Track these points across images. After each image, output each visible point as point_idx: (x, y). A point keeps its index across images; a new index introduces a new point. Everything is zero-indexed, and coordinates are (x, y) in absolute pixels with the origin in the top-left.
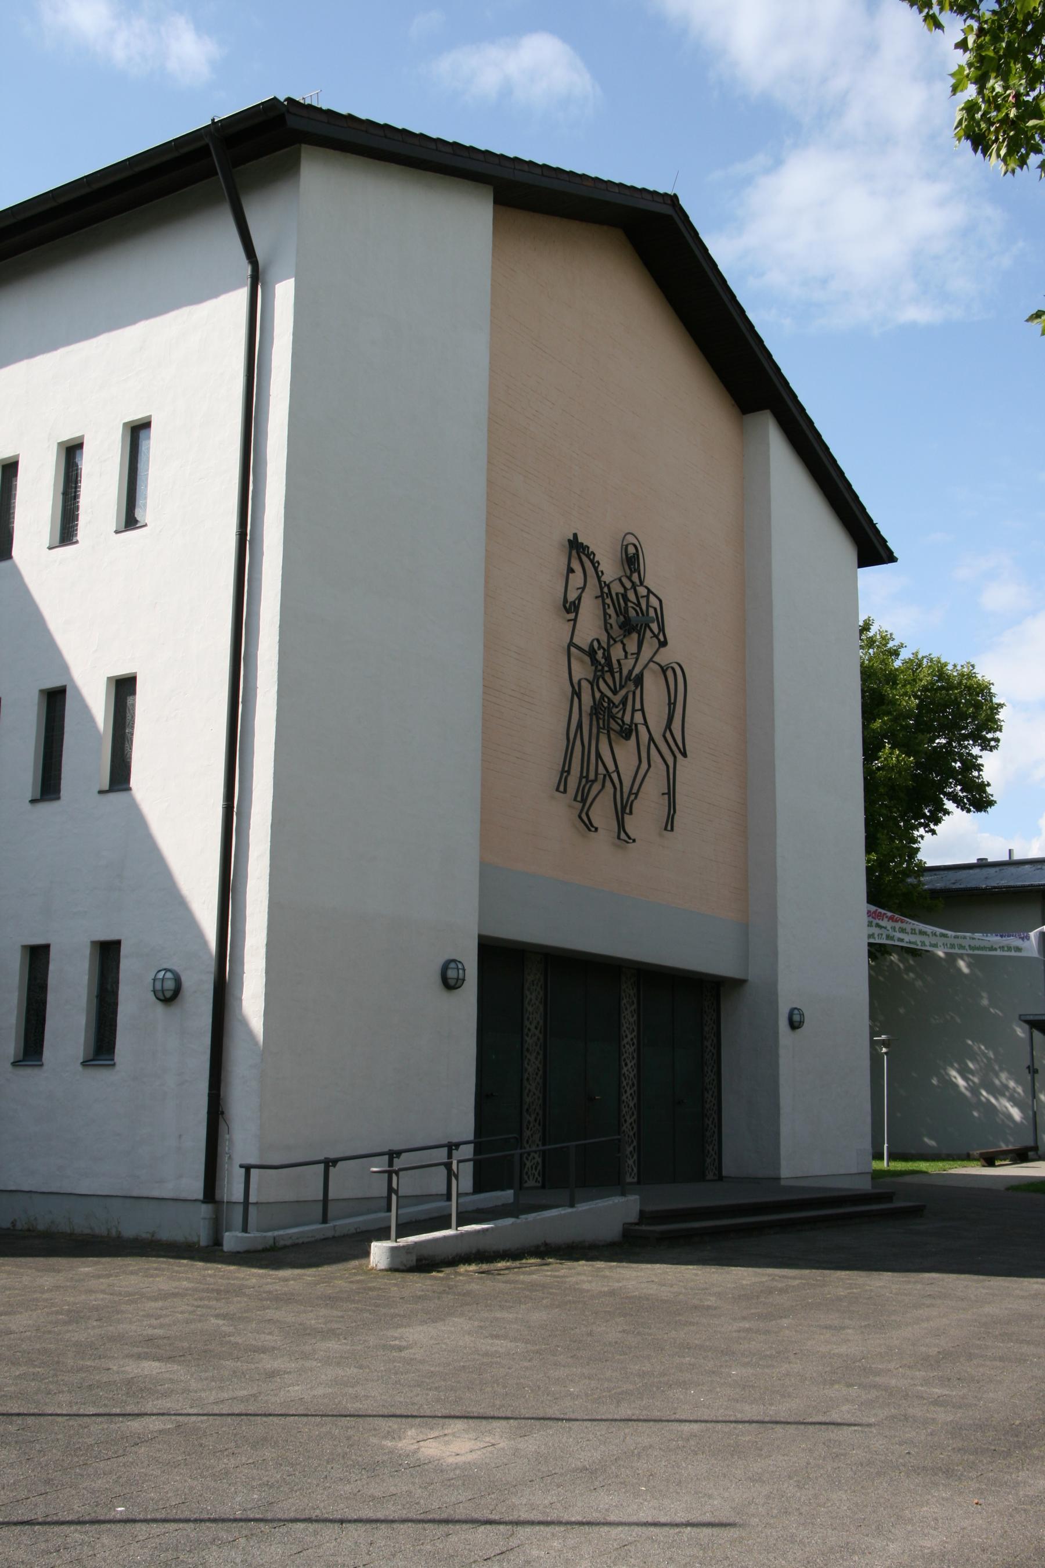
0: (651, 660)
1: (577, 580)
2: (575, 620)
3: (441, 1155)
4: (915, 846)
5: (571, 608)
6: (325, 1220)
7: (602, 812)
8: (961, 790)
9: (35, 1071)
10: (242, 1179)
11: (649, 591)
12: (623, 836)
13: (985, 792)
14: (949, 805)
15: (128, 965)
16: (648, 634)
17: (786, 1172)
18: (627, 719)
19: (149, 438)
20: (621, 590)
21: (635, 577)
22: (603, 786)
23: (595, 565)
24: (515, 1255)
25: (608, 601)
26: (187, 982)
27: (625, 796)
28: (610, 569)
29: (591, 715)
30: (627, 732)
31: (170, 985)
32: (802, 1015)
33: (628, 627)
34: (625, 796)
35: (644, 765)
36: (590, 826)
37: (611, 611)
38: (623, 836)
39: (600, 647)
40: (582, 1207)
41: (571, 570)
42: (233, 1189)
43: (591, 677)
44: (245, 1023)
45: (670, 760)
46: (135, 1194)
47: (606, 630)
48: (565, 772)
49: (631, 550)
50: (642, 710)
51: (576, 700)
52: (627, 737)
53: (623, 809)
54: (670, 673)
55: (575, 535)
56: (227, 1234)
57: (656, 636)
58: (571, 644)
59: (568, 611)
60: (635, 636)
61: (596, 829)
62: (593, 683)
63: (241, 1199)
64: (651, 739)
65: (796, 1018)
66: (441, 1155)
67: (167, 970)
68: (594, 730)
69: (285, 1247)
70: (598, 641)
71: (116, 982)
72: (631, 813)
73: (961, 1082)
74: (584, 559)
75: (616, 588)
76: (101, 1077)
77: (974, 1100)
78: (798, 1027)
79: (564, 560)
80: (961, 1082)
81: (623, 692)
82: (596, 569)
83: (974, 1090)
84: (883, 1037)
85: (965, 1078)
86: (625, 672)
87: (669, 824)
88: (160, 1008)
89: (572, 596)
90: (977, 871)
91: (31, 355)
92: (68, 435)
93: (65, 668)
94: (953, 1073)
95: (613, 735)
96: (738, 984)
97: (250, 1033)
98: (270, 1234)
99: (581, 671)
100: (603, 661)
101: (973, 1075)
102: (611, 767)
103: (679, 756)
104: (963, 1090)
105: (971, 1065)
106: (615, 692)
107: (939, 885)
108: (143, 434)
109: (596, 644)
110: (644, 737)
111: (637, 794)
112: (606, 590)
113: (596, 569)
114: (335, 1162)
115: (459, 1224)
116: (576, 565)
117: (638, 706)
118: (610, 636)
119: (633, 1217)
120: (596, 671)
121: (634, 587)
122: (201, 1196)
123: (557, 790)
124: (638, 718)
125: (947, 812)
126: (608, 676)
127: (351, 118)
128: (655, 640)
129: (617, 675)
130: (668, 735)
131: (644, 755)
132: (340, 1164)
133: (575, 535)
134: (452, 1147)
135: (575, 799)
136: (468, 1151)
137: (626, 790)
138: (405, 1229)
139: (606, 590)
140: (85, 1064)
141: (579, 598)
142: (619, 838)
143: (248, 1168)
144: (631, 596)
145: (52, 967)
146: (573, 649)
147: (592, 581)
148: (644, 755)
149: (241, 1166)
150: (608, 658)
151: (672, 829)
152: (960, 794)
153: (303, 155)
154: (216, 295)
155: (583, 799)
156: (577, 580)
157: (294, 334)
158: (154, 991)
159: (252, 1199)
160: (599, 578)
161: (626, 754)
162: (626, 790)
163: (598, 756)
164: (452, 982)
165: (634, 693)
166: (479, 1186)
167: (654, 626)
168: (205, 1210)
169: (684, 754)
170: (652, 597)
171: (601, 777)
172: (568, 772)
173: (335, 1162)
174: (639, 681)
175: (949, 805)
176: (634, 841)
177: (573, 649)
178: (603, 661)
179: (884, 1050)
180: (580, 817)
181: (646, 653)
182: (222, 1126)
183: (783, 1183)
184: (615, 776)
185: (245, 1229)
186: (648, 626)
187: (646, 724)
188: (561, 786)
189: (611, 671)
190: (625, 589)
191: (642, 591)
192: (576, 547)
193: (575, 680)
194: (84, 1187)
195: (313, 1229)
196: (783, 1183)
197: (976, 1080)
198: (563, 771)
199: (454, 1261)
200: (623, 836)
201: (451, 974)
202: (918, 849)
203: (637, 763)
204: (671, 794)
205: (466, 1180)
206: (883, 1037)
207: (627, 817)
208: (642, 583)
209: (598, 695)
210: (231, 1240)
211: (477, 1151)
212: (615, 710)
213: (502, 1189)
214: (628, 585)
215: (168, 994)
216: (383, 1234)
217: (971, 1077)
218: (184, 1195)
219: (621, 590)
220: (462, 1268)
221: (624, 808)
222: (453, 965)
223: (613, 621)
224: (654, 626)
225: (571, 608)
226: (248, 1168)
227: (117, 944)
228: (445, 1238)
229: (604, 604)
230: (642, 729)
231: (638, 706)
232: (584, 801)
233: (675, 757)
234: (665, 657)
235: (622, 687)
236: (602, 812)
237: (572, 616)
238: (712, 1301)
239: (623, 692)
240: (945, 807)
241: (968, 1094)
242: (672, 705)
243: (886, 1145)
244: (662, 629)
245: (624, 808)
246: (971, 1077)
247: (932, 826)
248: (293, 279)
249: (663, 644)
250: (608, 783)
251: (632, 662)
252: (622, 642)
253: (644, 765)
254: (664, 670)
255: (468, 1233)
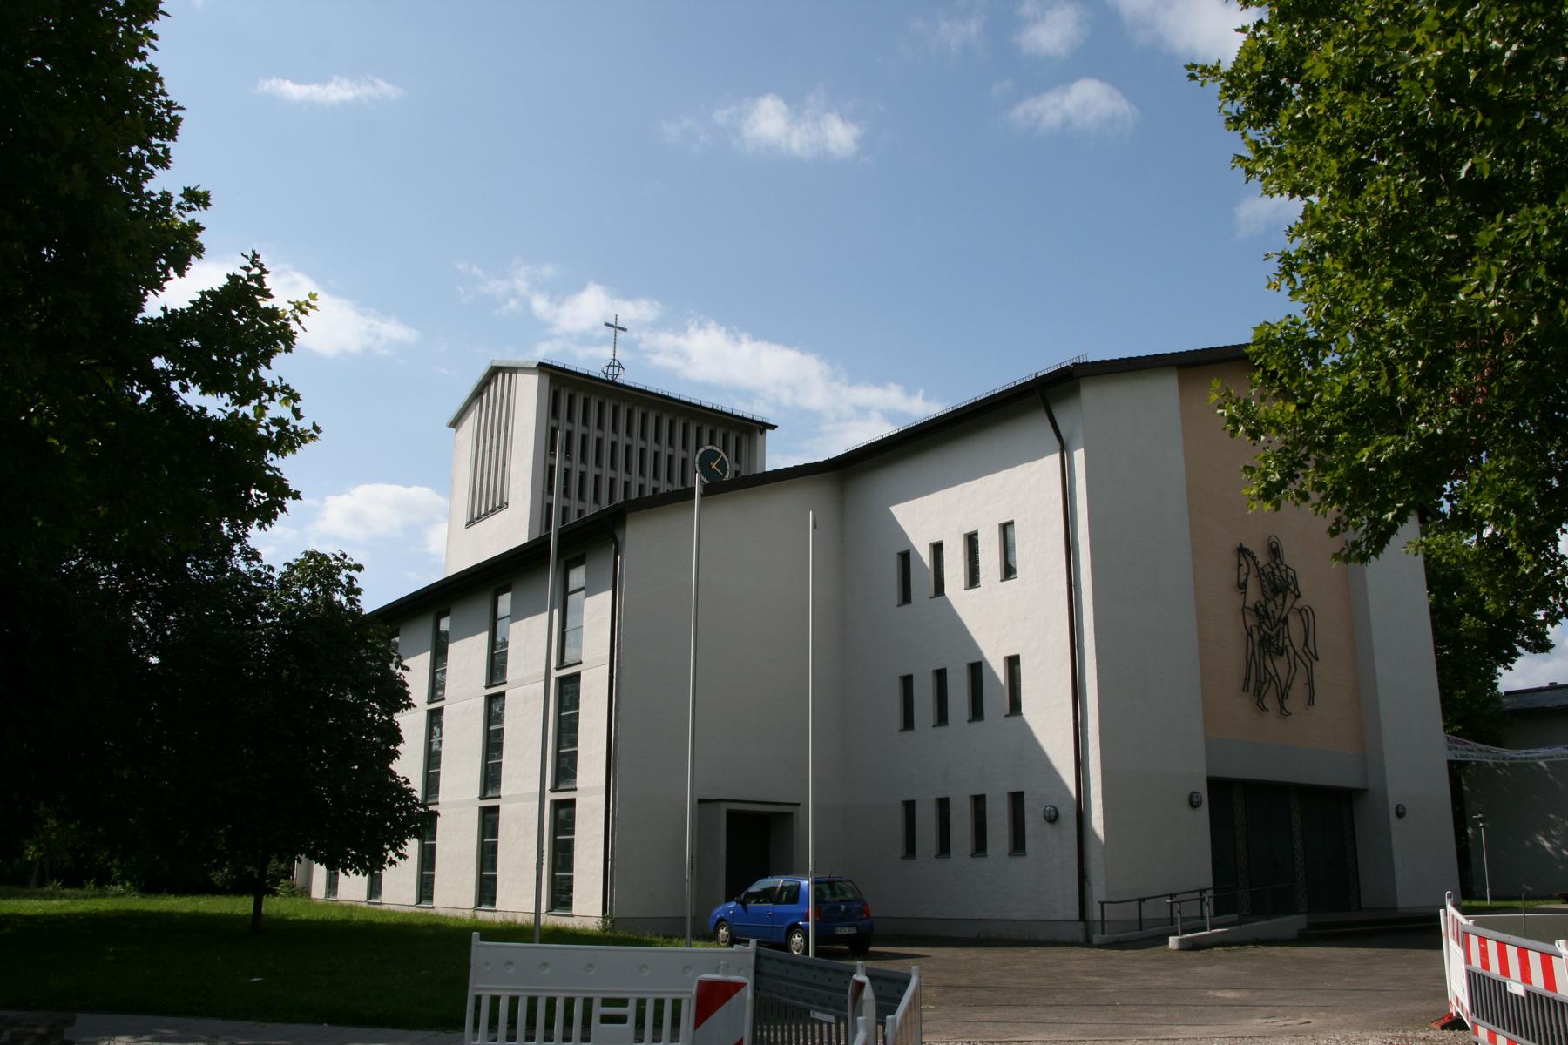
0: (1292, 607)
1: (1244, 569)
2: (1245, 593)
3: (1197, 895)
4: (1495, 681)
5: (1242, 586)
6: (1140, 930)
7: (1270, 701)
8: (1528, 639)
9: (983, 859)
10: (1100, 909)
11: (1287, 567)
12: (1284, 712)
13: (1546, 638)
14: (1520, 649)
15: (1029, 804)
16: (1288, 592)
17: (1401, 904)
18: (1280, 644)
19: (1013, 530)
20: (1270, 570)
21: (1278, 561)
22: (1270, 684)
23: (1254, 558)
24: (1242, 944)
25: (1263, 578)
26: (1062, 811)
27: (1283, 688)
28: (1262, 558)
29: (1259, 645)
30: (1281, 652)
31: (1053, 814)
32: (1404, 809)
33: (1276, 590)
34: (1283, 688)
35: (1293, 669)
36: (1264, 709)
37: (1266, 584)
38: (1283, 711)
39: (1261, 605)
40: (1275, 920)
41: (1240, 565)
42: (1095, 914)
43: (1256, 624)
44: (1093, 832)
45: (1309, 665)
46: (1042, 918)
47: (1264, 595)
48: (1247, 680)
49: (1274, 545)
50: (1289, 637)
51: (1250, 639)
52: (1282, 655)
53: (1282, 696)
54: (1304, 613)
55: (1241, 545)
56: (1094, 936)
57: (1294, 593)
58: (1244, 607)
59: (1241, 589)
60: (1281, 595)
61: (1268, 710)
62: (1259, 627)
63: (1100, 919)
64: (1296, 653)
65: (1401, 811)
66: (1197, 895)
67: (1051, 806)
68: (1262, 653)
69: (1123, 942)
70: (1259, 602)
71: (1023, 813)
72: (1287, 698)
73: (1547, 845)
74: (1247, 556)
75: (1268, 569)
76: (1018, 861)
77: (1558, 857)
78: (1403, 816)
79: (1236, 559)
80: (1547, 845)
81: (1275, 630)
82: (1254, 561)
83: (1558, 850)
84: (1480, 815)
85: (1551, 842)
86: (1277, 617)
87: (1311, 701)
88: (1048, 826)
89: (1242, 579)
90: (1548, 692)
91: (944, 488)
92: (969, 530)
93: (980, 652)
94: (1541, 838)
95: (1273, 655)
96: (1365, 790)
97: (1096, 836)
98: (1116, 936)
99: (1251, 621)
100: (1263, 613)
101: (1557, 839)
102: (1273, 673)
103: (1313, 660)
104: (1549, 850)
105: (1554, 833)
106: (1272, 630)
107: (1519, 705)
108: (1009, 528)
109: (1258, 604)
110: (1291, 652)
111: (1290, 687)
112: (1261, 572)
113: (1254, 561)
114: (1144, 900)
115: (1211, 929)
116: (1243, 561)
117: (1286, 635)
118: (1266, 598)
119: (1304, 926)
120: (1260, 619)
121: (1278, 567)
122: (1078, 918)
123: (1244, 690)
124: (1287, 642)
125: (1519, 655)
126: (1267, 622)
127: (1103, 361)
128: (1293, 595)
129: (1272, 620)
130: (1306, 650)
131: (1292, 662)
132: (1147, 901)
133: (1241, 545)
134: (1202, 891)
135: (1254, 694)
136: (1210, 893)
137: (1283, 685)
138: (1184, 932)
139: (1261, 572)
140: (972, 856)
141: (1246, 580)
142: (1281, 713)
143: (1102, 904)
144: (1277, 572)
145: (987, 806)
146: (1246, 610)
147: (1253, 567)
148: (1292, 662)
149: (1099, 902)
150: (1266, 611)
151: (1313, 704)
152: (1527, 641)
153: (1082, 385)
154: (1042, 457)
155: (1259, 695)
156: (1244, 569)
157: (1087, 477)
158: (1045, 817)
159: (1105, 919)
160: (1257, 566)
161: (1281, 665)
162: (1283, 685)
163: (1266, 668)
164: (1195, 804)
165: (1283, 628)
166: (1218, 912)
167: (1292, 588)
168: (1081, 925)
169: (1317, 659)
170: (1289, 570)
171: (1268, 680)
172: (1249, 680)
173: (1144, 900)
174: (1286, 621)
175: (1520, 649)
176: (1290, 714)
177: (1246, 610)
178: (1263, 613)
179: (1481, 824)
180: (1257, 704)
181: (1288, 603)
182: (1086, 884)
183: (1399, 910)
184: (1276, 678)
185: (1103, 933)
186: (1288, 587)
187: (1292, 645)
188: (1246, 688)
189: (1269, 618)
190: (1273, 569)
191: (1283, 568)
192: (1242, 551)
193: (1248, 626)
194: (1014, 916)
195: (1135, 934)
196: (1399, 910)
197: (1558, 842)
198: (1246, 679)
199: (1211, 946)
200: (1283, 711)
201: (1195, 799)
202: (1497, 684)
203: (1288, 668)
204: (1310, 684)
205: (1209, 911)
206: (1480, 815)
207: (1286, 701)
208: (1282, 563)
209: (1262, 633)
210: (1096, 938)
211: (1214, 893)
212: (1273, 641)
213: (1229, 913)
214: (1274, 566)
215: (1053, 818)
216: (1175, 934)
217: (1554, 841)
218: (1068, 918)
219: (1270, 570)
220: (1215, 949)
221: (1283, 696)
222: (1195, 795)
223: (1267, 589)
224: (1292, 588)
225: (1242, 586)
226: (1102, 904)
227: (1021, 794)
228: (1205, 935)
229: (1261, 580)
230: (1290, 648)
231: (1286, 635)
232: (1259, 695)
233: (1311, 662)
234: (1299, 603)
235: (1275, 626)
236: (1270, 701)
237: (1243, 591)
238: (1342, 959)
239: (1275, 630)
240: (1500, 669)
241: (1553, 852)
242: (1306, 631)
243: (1488, 890)
244: (1296, 588)
245: (1283, 696)
246: (1554, 841)
247: (1509, 664)
248: (1082, 450)
249: (1298, 596)
250: (1272, 683)
251: (1280, 610)
252: (1273, 600)
253: (1293, 669)
254: (1299, 611)
255: (1216, 933)
